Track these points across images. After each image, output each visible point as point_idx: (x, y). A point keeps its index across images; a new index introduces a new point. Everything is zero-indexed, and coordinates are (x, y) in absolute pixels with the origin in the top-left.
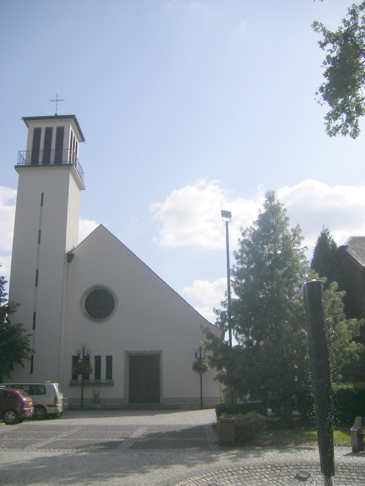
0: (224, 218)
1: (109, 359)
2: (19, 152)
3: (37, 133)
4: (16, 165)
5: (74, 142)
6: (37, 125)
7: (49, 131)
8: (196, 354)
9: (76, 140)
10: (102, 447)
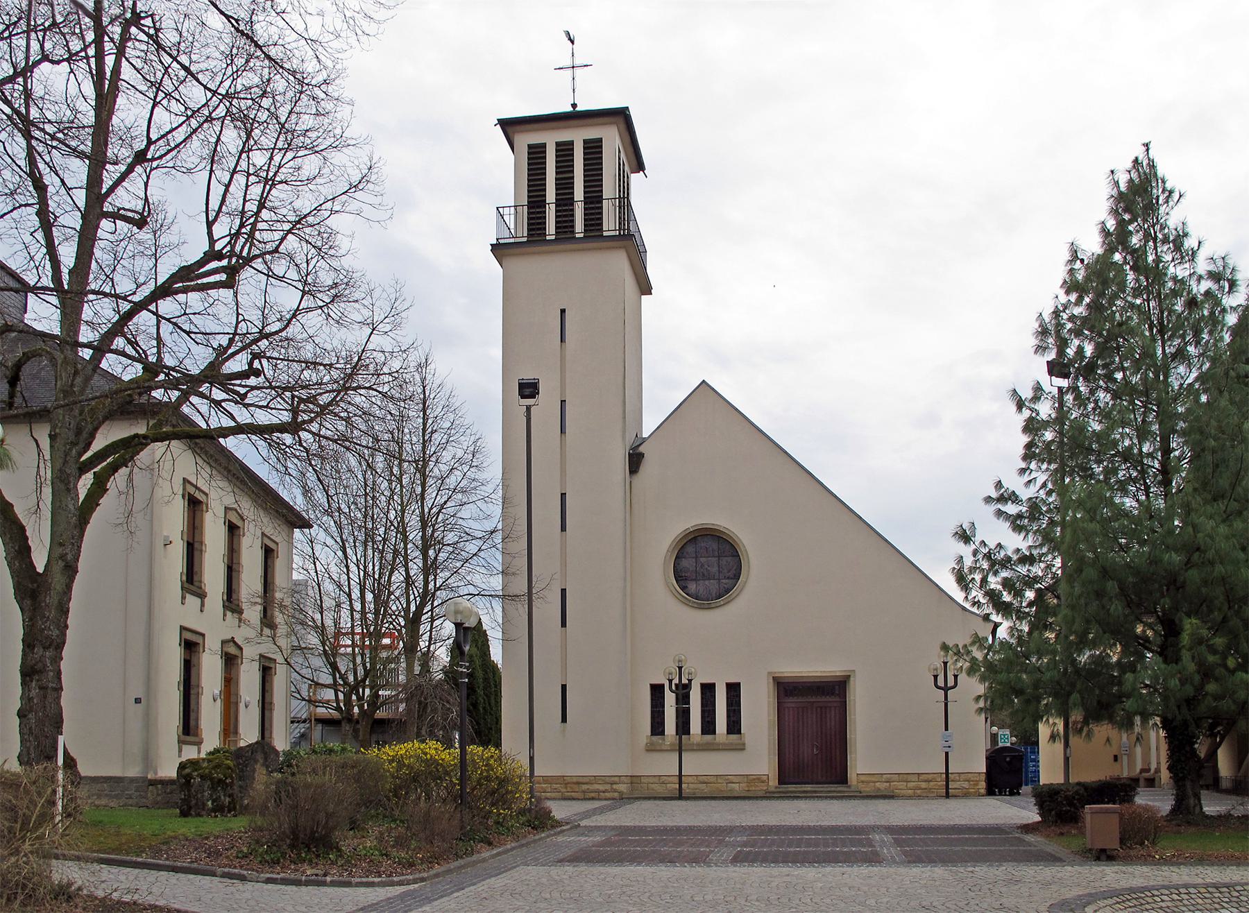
0: (1053, 377)
1: (733, 690)
2: (497, 208)
3: (536, 155)
4: (495, 242)
5: (624, 171)
6: (536, 138)
7: (565, 151)
8: (936, 677)
9: (627, 168)
10: (829, 738)
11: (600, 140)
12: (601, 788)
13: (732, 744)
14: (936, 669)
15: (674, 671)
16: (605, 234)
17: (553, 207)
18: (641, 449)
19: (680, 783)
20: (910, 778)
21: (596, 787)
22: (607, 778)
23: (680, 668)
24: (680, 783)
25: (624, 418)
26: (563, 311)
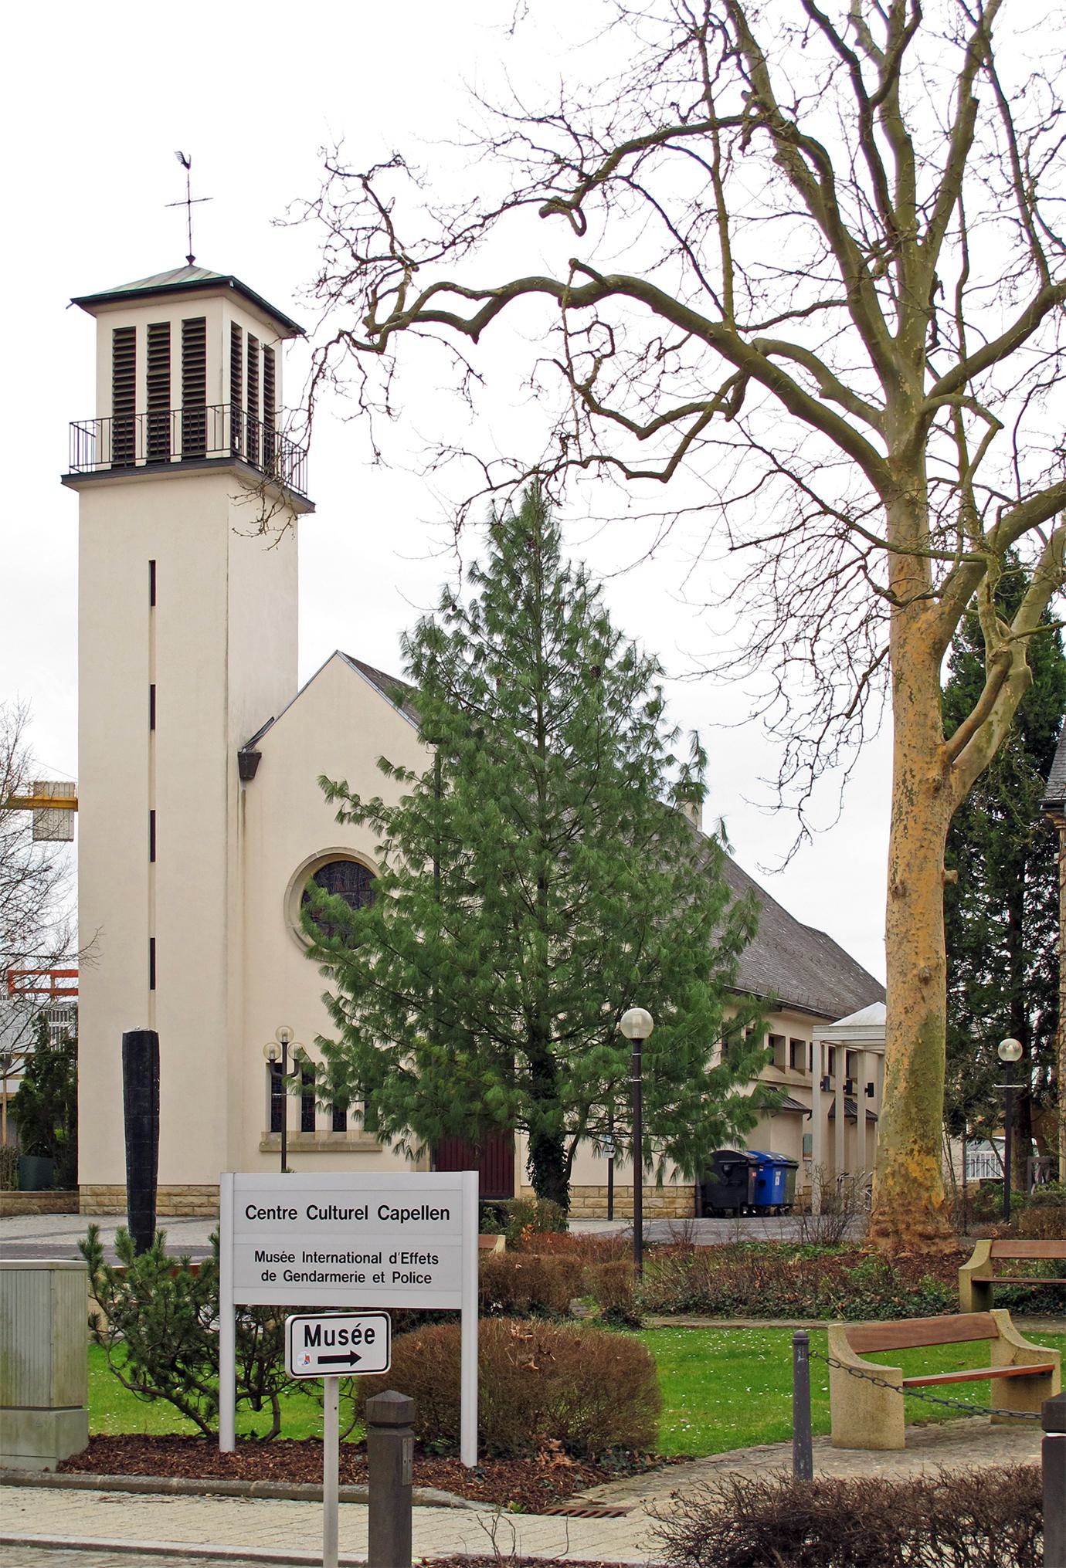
3: (124, 340)
7: (159, 334)
11: (203, 320)
12: (196, 1201)
13: (365, 1144)
14: (273, 1052)
15: (276, 1049)
16: (209, 455)
17: (179, 415)
18: (259, 747)
19: (611, 1196)
20: (589, 1191)
21: (190, 1199)
22: (204, 1189)
23: (285, 1044)
24: (611, 1196)
25: (226, 708)
26: (153, 563)
